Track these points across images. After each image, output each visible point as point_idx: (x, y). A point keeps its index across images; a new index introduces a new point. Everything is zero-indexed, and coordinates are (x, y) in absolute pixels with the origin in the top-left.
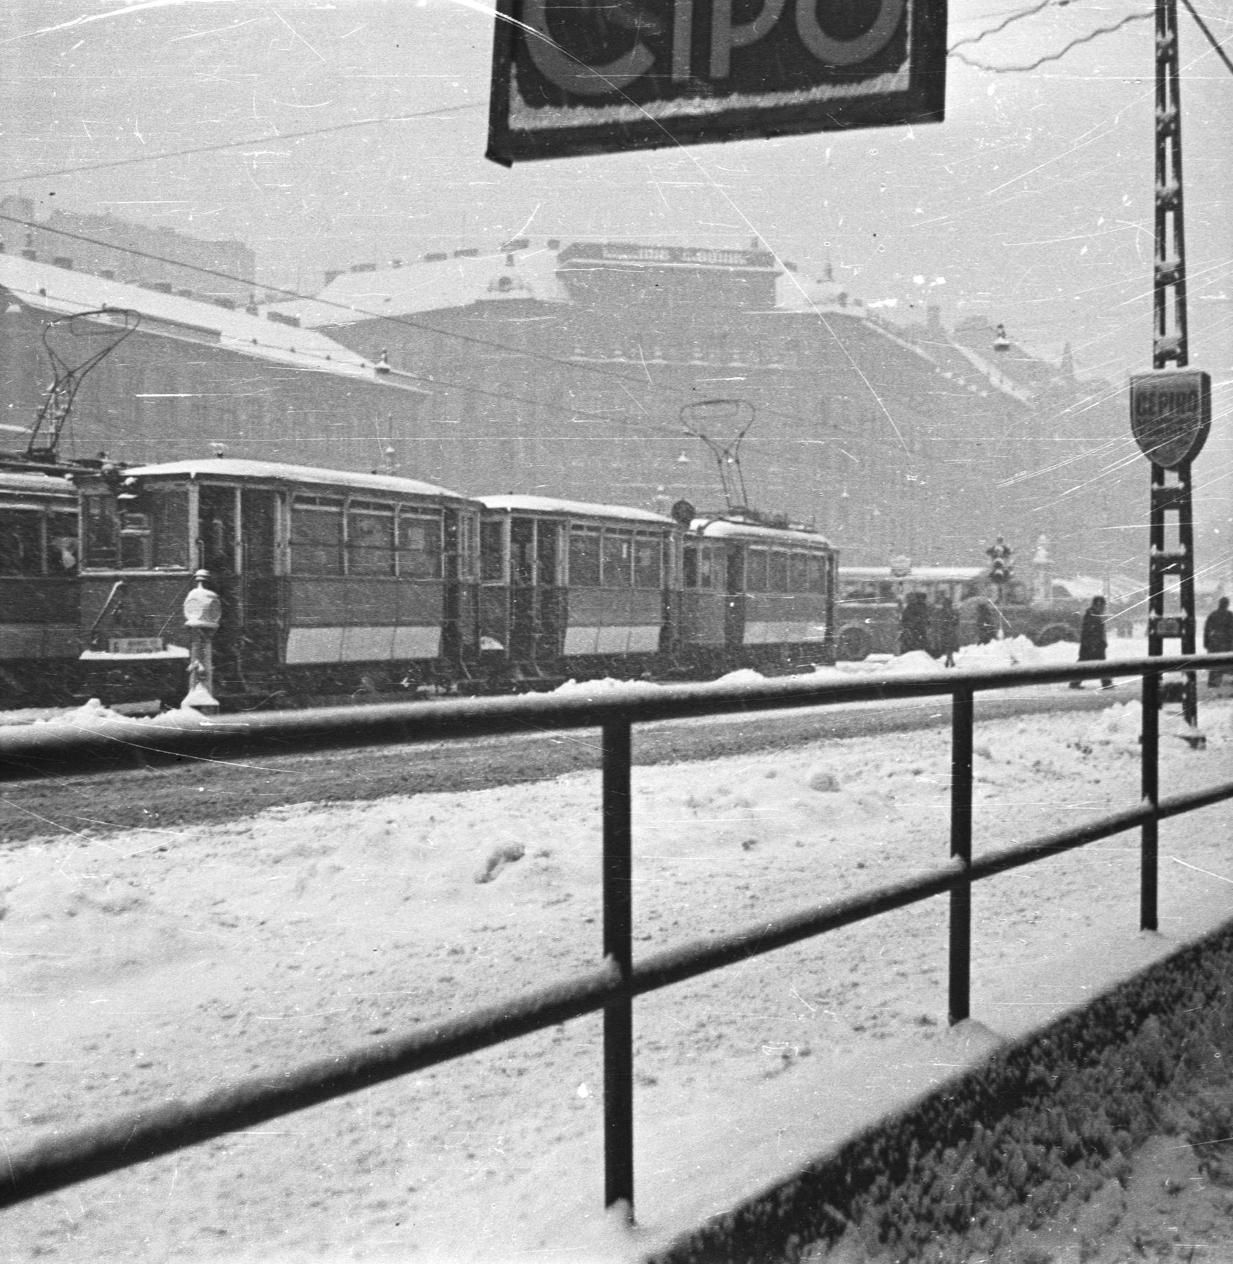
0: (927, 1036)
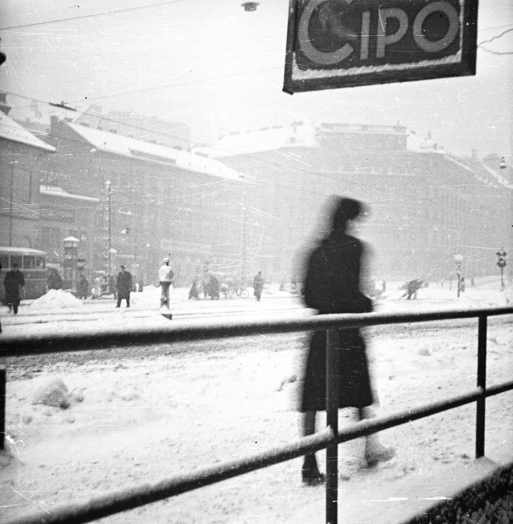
0: (466, 463)
